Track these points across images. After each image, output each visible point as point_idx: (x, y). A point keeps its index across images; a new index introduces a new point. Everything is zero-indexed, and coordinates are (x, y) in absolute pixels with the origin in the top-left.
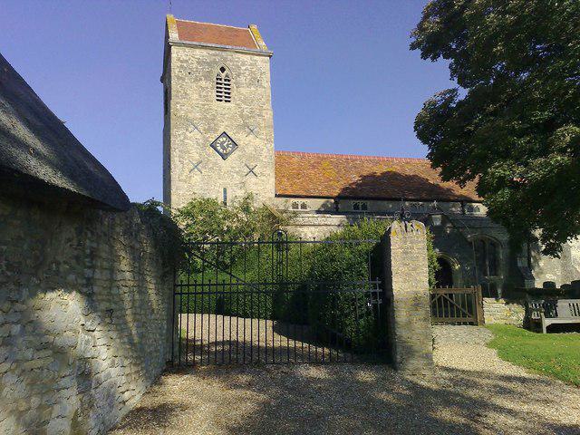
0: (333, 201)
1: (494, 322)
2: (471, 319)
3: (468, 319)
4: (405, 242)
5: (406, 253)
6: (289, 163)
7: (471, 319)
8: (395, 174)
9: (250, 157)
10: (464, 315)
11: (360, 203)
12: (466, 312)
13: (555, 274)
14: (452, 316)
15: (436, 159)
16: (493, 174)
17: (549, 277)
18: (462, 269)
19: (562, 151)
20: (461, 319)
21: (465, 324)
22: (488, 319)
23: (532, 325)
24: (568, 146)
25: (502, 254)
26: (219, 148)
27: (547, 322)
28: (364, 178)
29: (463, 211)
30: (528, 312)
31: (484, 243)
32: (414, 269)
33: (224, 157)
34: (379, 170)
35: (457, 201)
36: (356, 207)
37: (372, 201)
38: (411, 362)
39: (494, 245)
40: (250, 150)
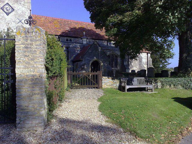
0: (57, 37)
1: (106, 87)
2: (97, 86)
3: (96, 86)
4: (27, 40)
5: (26, 48)
6: (40, 20)
7: (97, 86)
8: (84, 28)
9: (20, 15)
10: (94, 84)
11: (69, 39)
12: (95, 83)
13: (137, 68)
14: (89, 85)
15: (93, 18)
16: (110, 20)
17: (134, 68)
18: (104, 65)
19: (139, 9)
20: (93, 86)
21: (94, 88)
22: (104, 86)
23: (121, 88)
24: (142, 6)
25: (119, 60)
26: (5, 10)
27: (127, 87)
28: (72, 29)
29: (107, 44)
30: (121, 83)
31: (113, 56)
32: (32, 60)
33: (8, 14)
34: (78, 26)
35: (105, 40)
36: (67, 40)
37: (74, 38)
38: (28, 122)
39: (116, 56)
40: (20, 12)
